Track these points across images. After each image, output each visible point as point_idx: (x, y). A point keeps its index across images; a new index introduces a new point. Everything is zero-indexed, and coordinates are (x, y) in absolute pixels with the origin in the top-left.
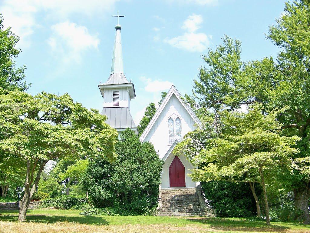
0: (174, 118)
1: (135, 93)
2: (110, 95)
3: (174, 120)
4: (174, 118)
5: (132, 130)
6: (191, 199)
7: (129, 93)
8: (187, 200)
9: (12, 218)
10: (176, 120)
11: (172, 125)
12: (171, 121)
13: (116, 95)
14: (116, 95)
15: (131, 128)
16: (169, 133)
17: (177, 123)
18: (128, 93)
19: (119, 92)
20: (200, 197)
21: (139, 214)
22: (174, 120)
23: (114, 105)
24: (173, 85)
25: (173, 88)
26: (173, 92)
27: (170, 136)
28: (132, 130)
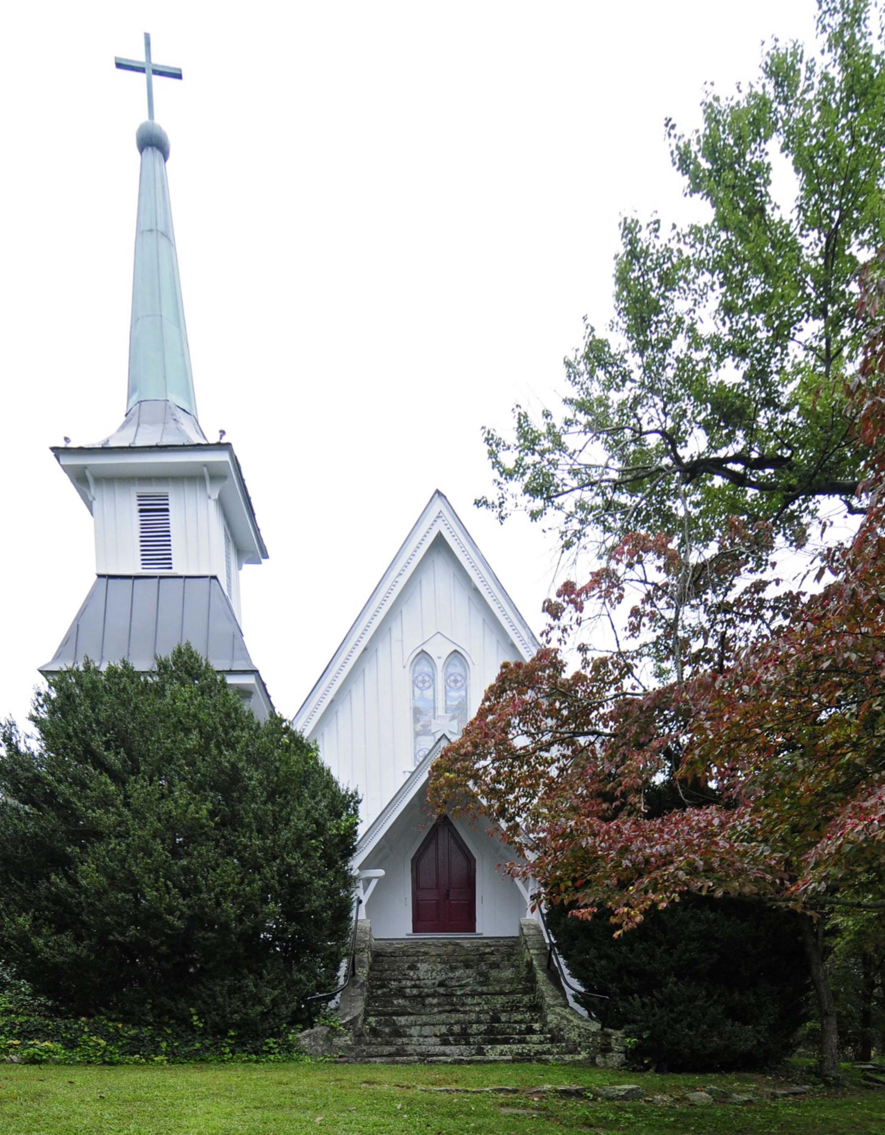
0: (439, 651)
1: (257, 530)
2: (125, 509)
3: (439, 663)
4: (439, 651)
5: (231, 680)
6: (498, 981)
7: (221, 502)
8: (481, 984)
9: (465, 1012)
10: (447, 665)
11: (427, 685)
12: (427, 669)
13: (153, 511)
14: (153, 511)
15: (231, 672)
16: (416, 720)
17: (452, 678)
18: (212, 507)
19: (165, 497)
20: (541, 976)
21: (198, 1059)
22: (439, 663)
23: (145, 562)
24: (438, 492)
25: (438, 505)
26: (440, 527)
27: (417, 734)
28: (231, 680)
